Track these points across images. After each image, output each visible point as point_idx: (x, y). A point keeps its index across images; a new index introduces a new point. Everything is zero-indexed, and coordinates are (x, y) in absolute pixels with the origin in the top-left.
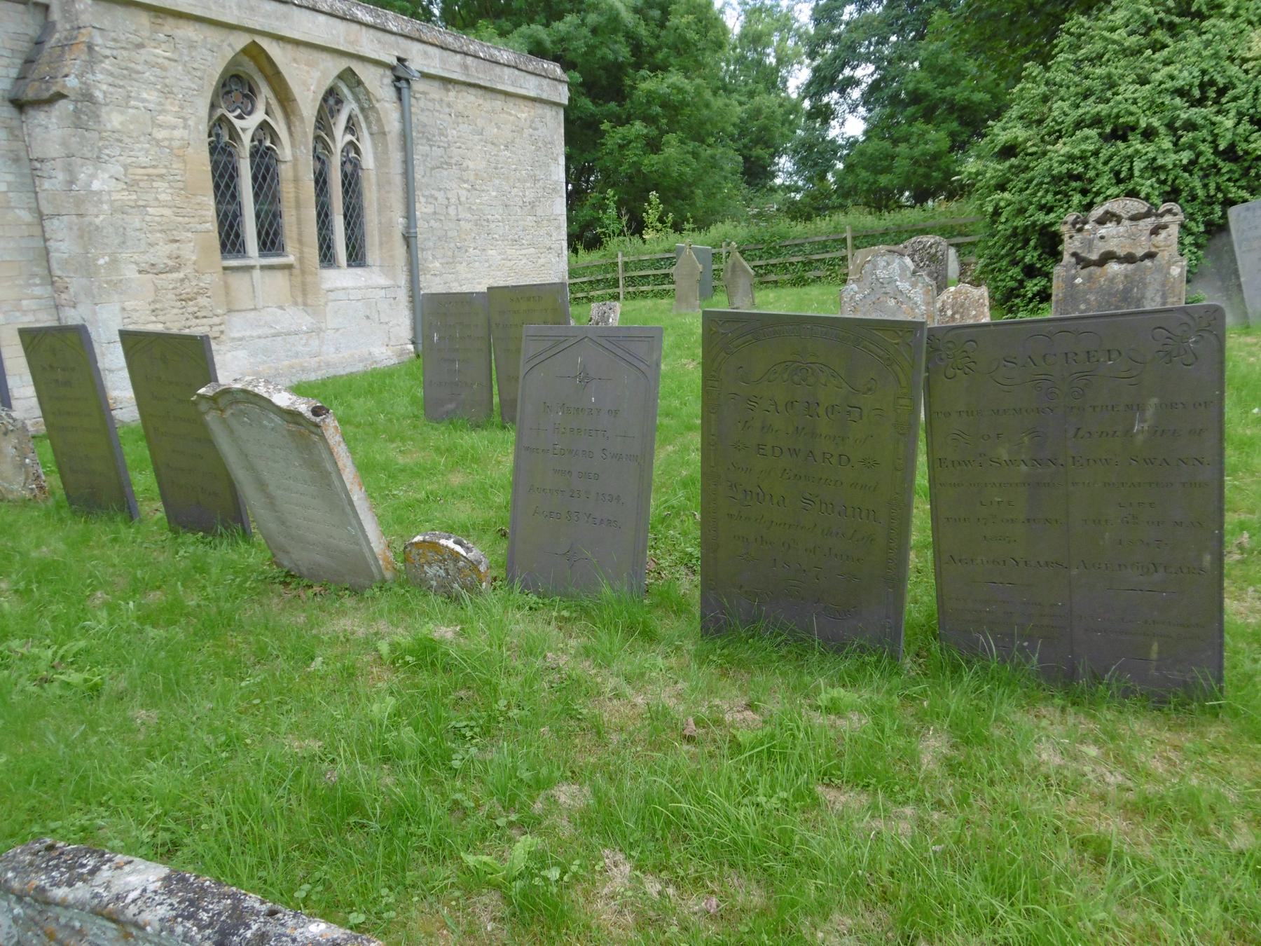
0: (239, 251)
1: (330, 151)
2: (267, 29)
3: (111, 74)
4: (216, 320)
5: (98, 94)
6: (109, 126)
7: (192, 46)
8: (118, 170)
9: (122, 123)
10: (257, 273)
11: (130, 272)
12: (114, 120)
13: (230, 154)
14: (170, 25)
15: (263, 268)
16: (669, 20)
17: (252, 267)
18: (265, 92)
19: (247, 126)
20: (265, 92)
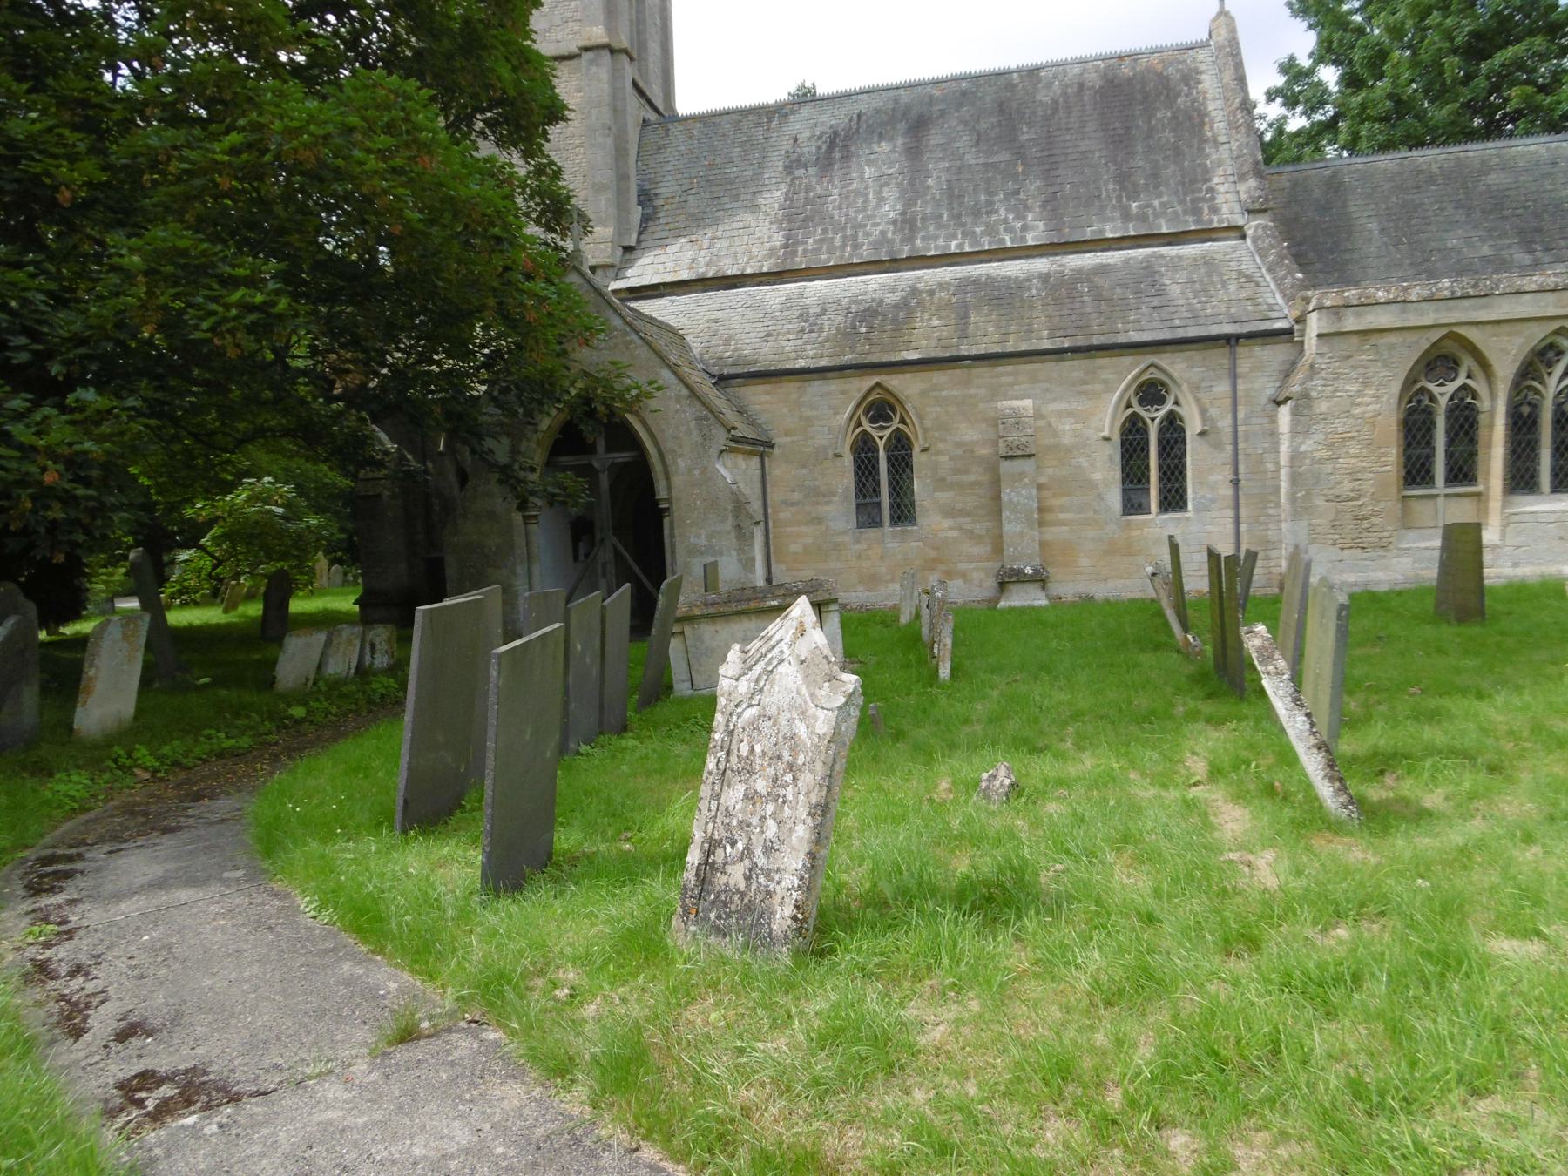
0: (1527, 484)
1: (1542, 397)
2: (1463, 320)
3: (1325, 379)
4: (1386, 534)
5: (1314, 394)
6: (1318, 411)
7: (1392, 347)
8: (1319, 437)
9: (1328, 408)
10: (1441, 500)
11: (1320, 502)
12: (1323, 407)
13: (1430, 413)
14: (1374, 339)
15: (1447, 495)
16: (86, 609)
17: (1437, 495)
18: (1467, 362)
19: (1444, 392)
20: (1467, 362)
